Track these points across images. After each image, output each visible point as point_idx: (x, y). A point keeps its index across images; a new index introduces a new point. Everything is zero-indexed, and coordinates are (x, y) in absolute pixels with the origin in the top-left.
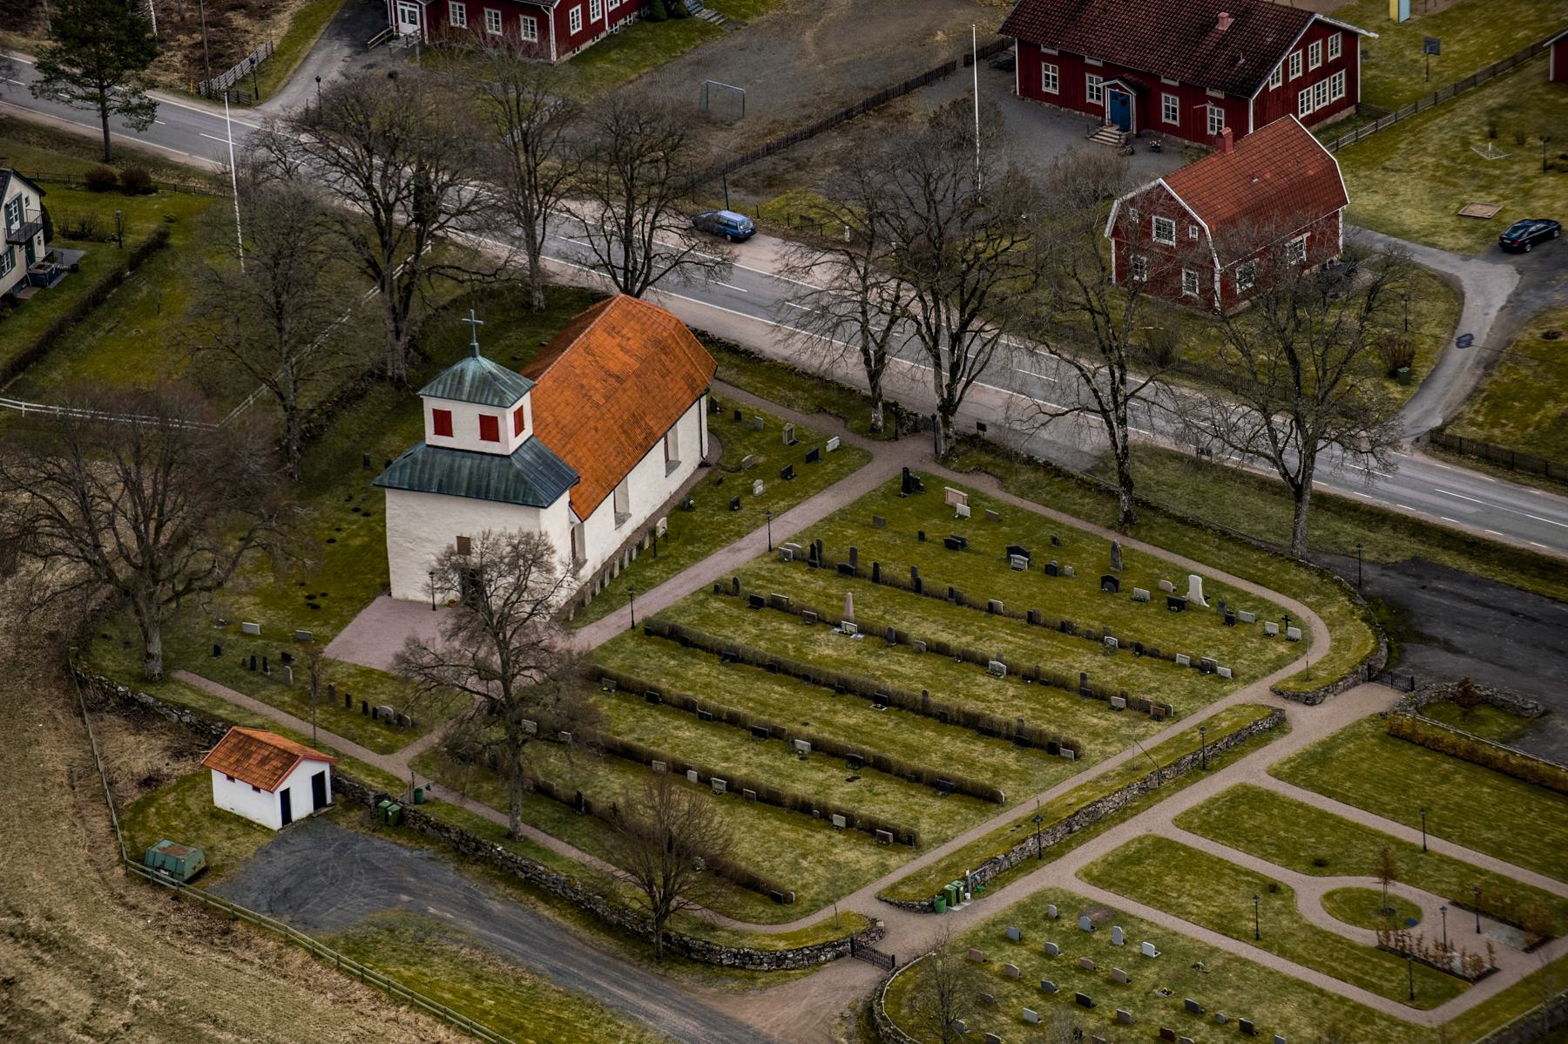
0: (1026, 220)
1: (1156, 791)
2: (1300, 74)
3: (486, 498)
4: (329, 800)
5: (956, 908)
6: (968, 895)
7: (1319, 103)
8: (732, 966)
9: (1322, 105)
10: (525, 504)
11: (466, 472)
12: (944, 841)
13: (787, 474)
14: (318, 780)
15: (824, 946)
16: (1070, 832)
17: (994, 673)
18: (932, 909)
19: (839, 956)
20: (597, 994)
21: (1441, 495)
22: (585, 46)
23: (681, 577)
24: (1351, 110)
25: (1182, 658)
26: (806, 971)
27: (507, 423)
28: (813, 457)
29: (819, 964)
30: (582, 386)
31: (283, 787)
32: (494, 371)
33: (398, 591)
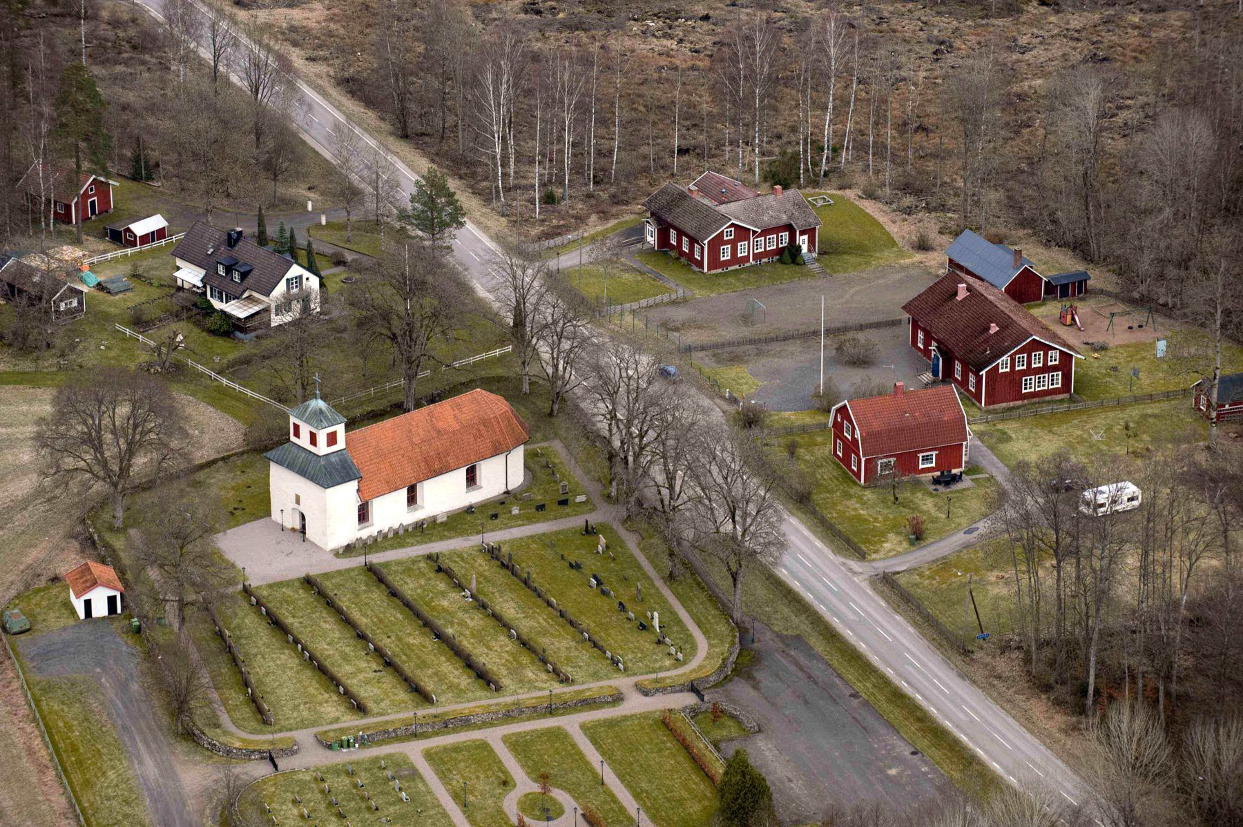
0: (107, 348)
1: (514, 718)
2: (1041, 365)
3: (304, 476)
4: (119, 610)
5: (344, 750)
6: (357, 745)
7: (1052, 384)
8: (207, 749)
9: (1042, 388)
10: (318, 484)
11: (301, 460)
12: (382, 715)
13: (541, 507)
14: (111, 600)
15: (255, 751)
16: (446, 727)
17: (510, 637)
18: (330, 747)
19: (262, 758)
20: (129, 743)
21: (849, 607)
22: (730, 268)
23: (424, 546)
24: (1066, 396)
25: (609, 654)
26: (1004, 788)
27: (322, 437)
28: (563, 503)
29: (250, 760)
30: (410, 431)
31: (87, 597)
32: (324, 409)
33: (276, 515)
